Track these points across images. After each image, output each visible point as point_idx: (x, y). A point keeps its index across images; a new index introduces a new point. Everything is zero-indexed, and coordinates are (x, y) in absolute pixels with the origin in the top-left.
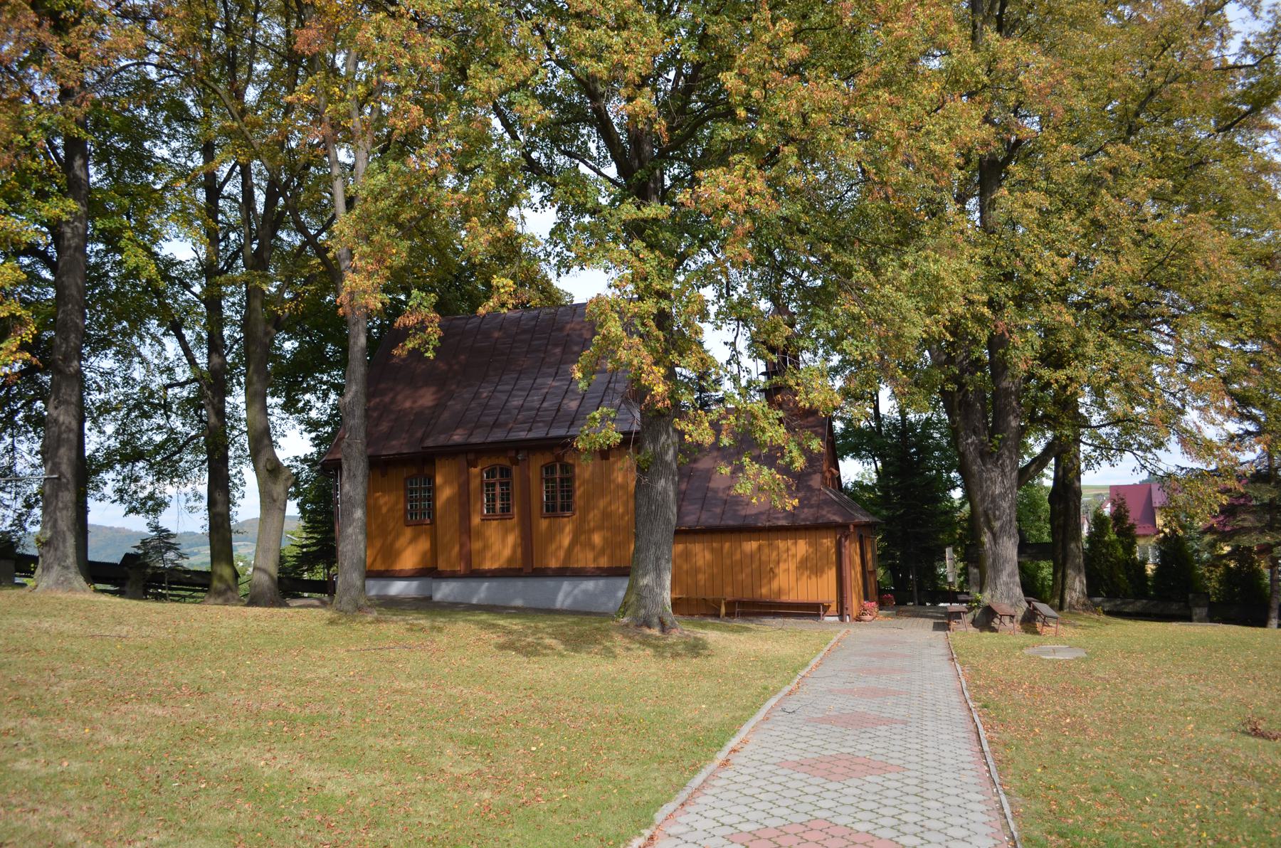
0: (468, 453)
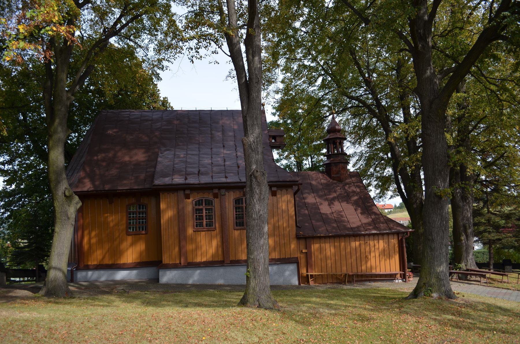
0: (186, 189)
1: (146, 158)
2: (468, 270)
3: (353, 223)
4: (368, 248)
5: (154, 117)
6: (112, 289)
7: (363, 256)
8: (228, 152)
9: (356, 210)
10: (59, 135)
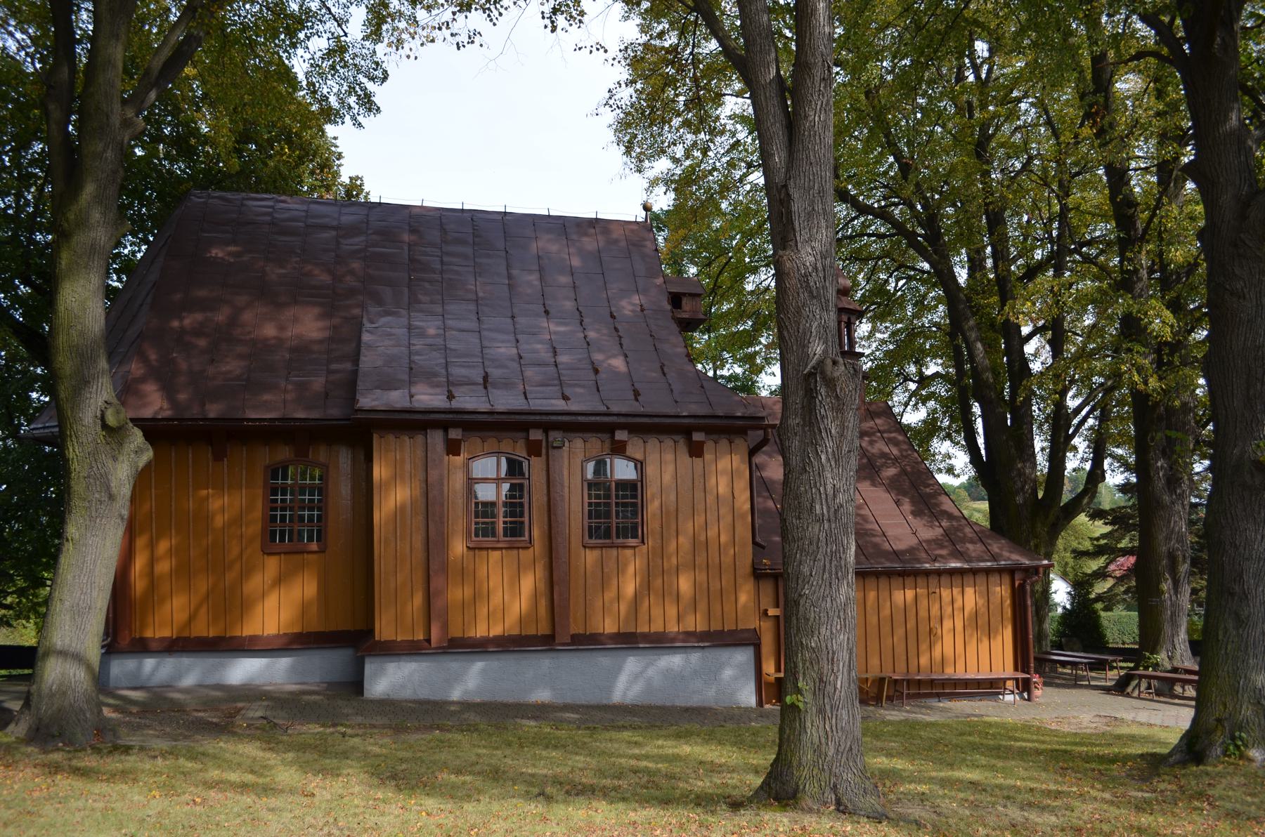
1: (326, 334)
2: (1175, 670)
3: (897, 538)
4: (937, 606)
5: (344, 219)
6: (223, 715)
7: (924, 629)
8: (562, 329)
9: (897, 503)
10: (92, 234)
